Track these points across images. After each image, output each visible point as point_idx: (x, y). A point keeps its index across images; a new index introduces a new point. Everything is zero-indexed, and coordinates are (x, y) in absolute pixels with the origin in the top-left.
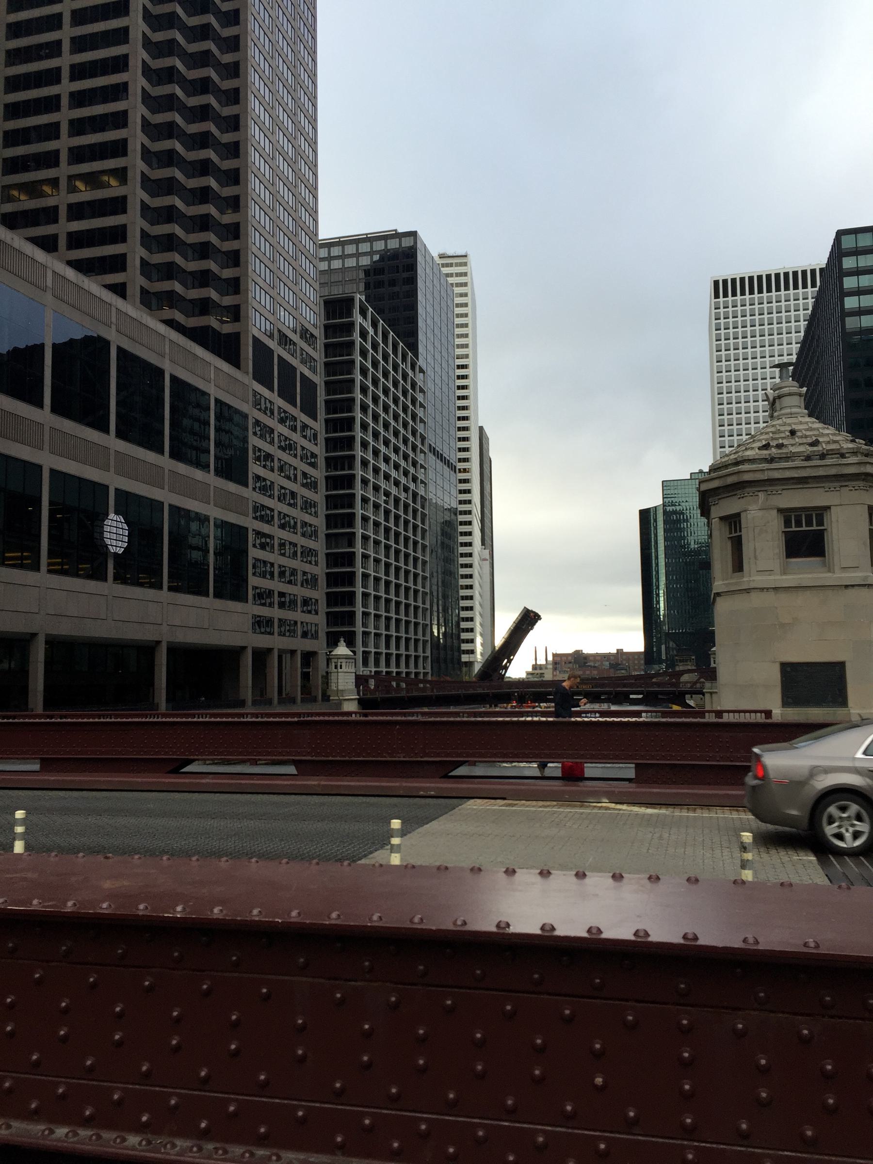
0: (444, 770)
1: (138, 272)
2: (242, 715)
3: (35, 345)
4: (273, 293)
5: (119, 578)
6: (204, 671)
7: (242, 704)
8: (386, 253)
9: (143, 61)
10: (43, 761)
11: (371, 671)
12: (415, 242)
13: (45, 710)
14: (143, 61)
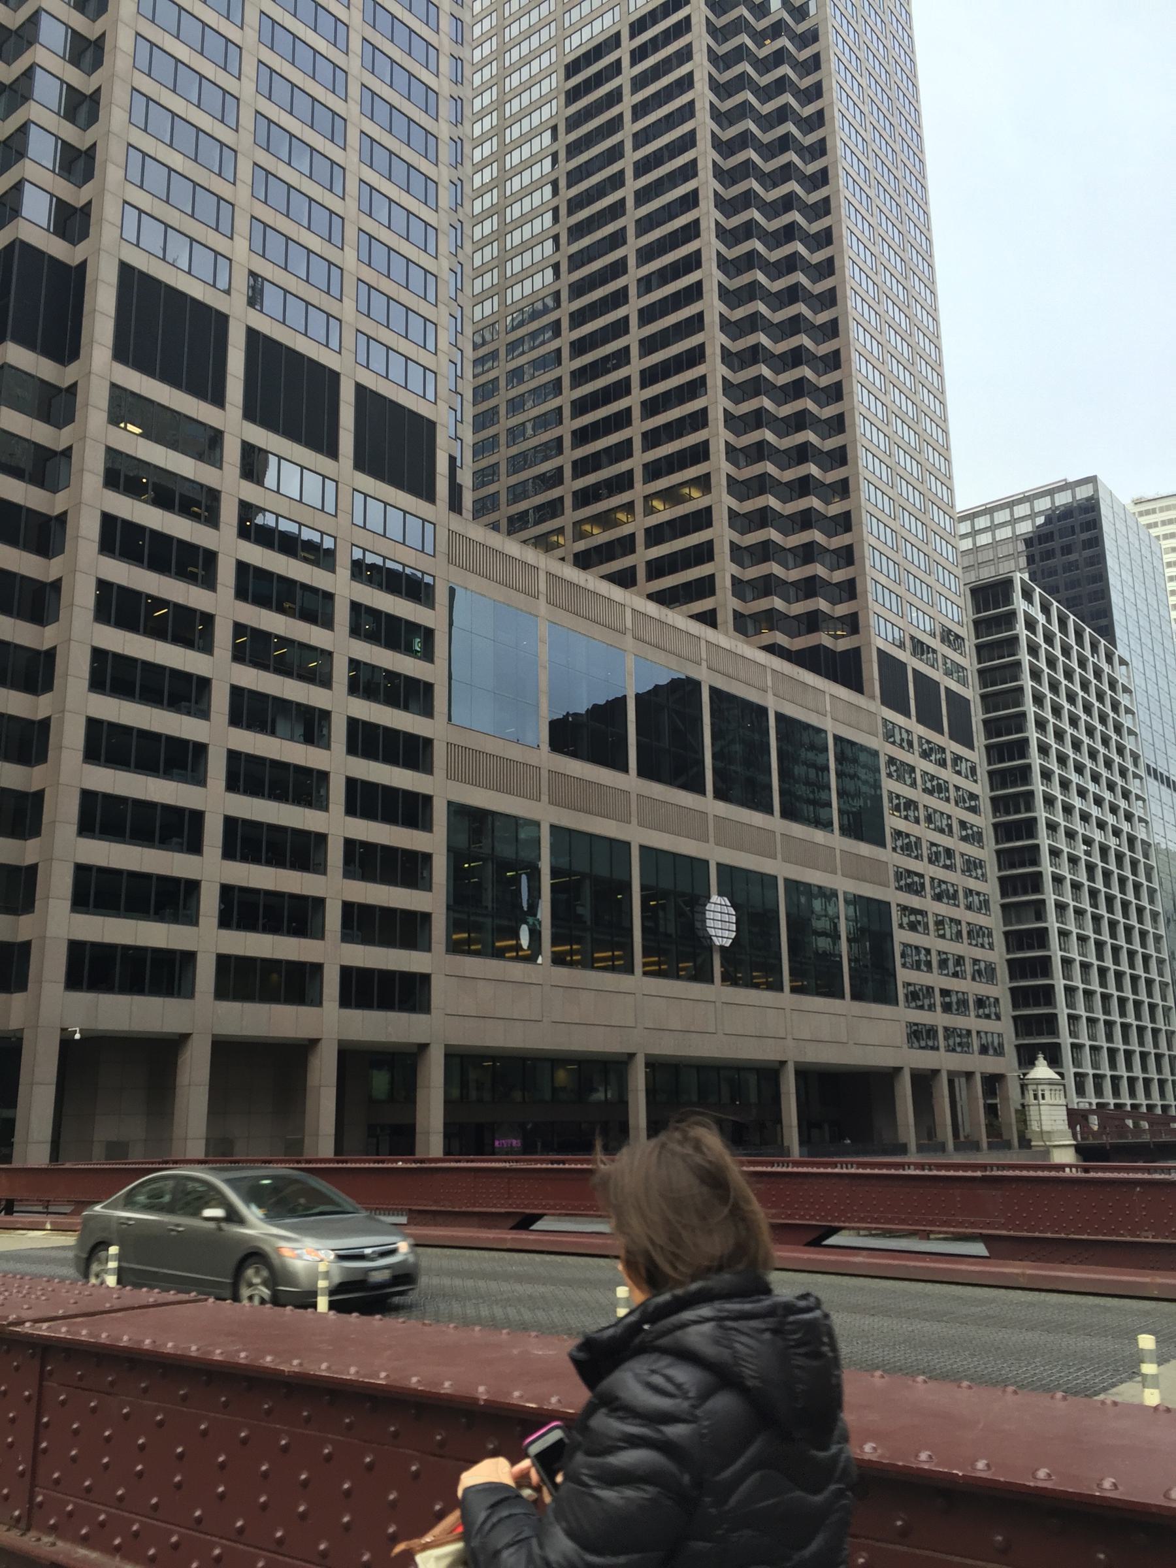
2: (902, 1166)
3: (617, 699)
4: (930, 580)
5: (730, 979)
8: (1054, 511)
11: (1090, 1104)
12: (1096, 490)
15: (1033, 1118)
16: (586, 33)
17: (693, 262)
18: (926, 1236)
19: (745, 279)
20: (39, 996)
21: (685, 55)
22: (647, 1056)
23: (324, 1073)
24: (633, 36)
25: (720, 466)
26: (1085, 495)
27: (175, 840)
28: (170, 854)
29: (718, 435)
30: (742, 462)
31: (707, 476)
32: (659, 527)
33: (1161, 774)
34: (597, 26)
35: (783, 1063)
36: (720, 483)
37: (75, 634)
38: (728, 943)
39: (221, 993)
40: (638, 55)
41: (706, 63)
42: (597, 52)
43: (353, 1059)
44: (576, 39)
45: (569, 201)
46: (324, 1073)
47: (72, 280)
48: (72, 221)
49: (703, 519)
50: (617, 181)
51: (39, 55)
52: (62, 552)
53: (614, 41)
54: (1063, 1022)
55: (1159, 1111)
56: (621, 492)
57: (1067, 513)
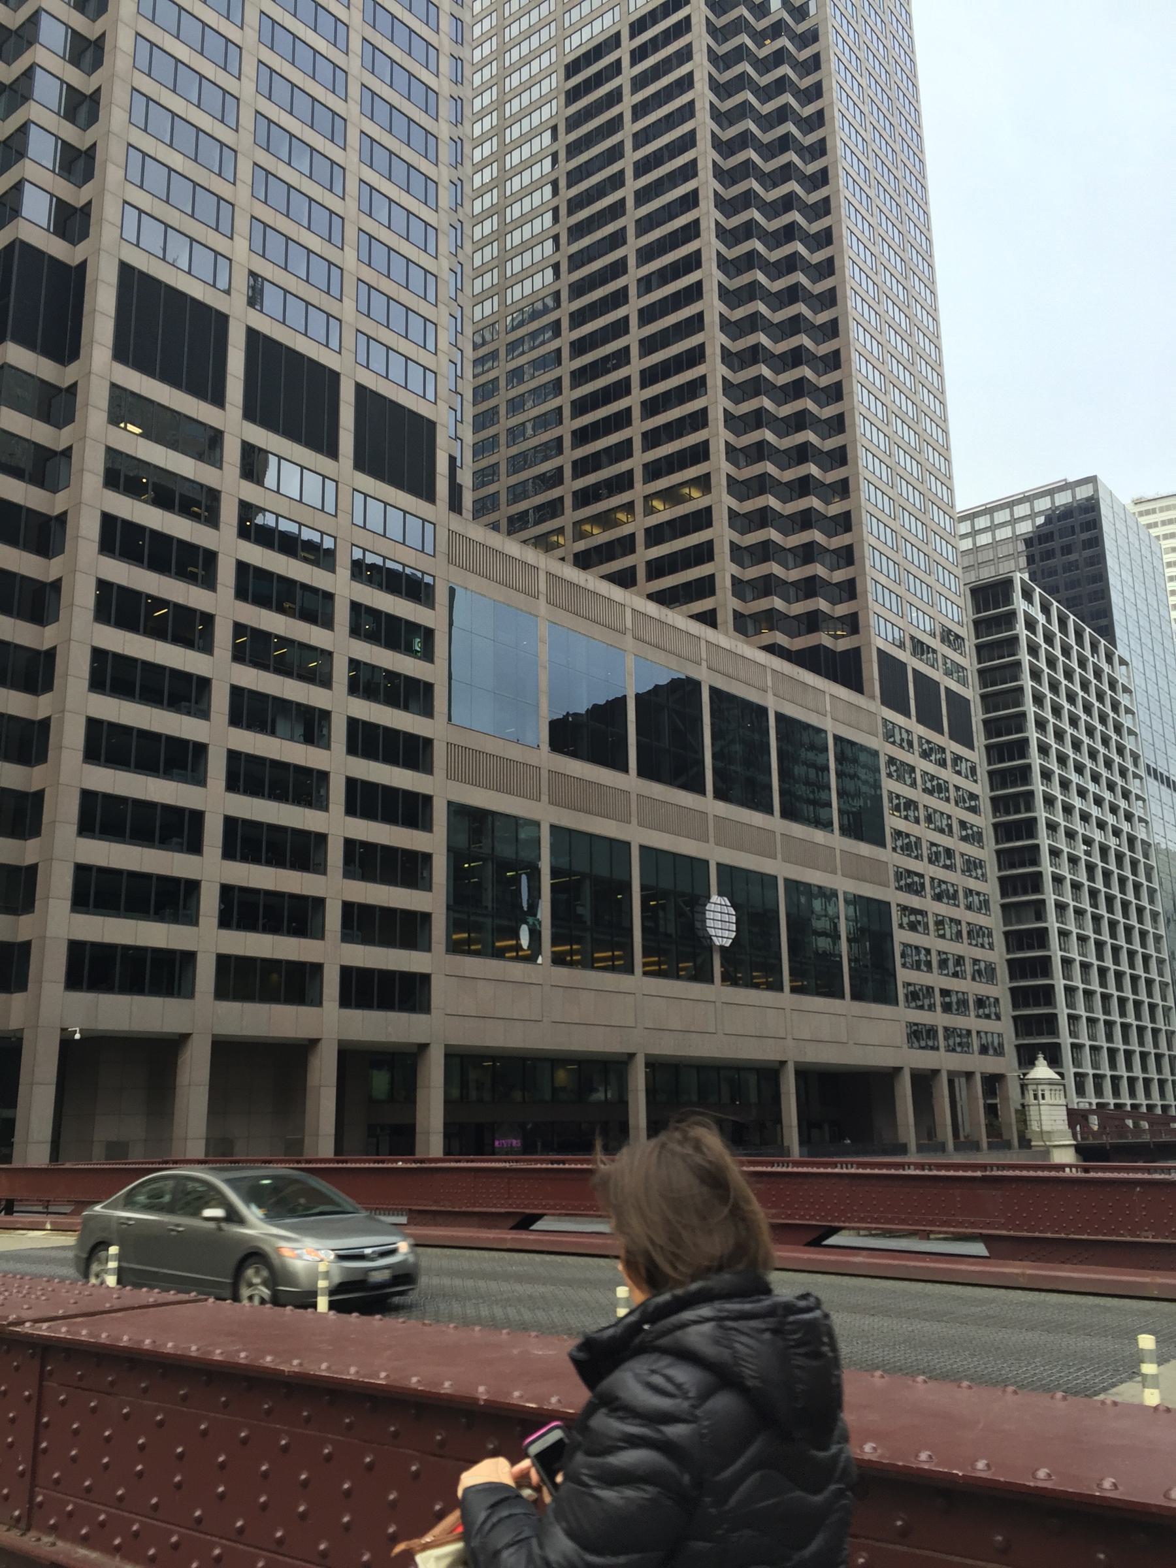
2: (902, 1166)
3: (617, 699)
4: (930, 580)
5: (730, 979)
8: (1054, 511)
11: (1090, 1104)
12: (1096, 490)
15: (1033, 1118)
16: (586, 33)
17: (693, 262)
18: (926, 1236)
19: (745, 279)
20: (39, 996)
21: (685, 55)
24: (633, 36)
25: (720, 466)
26: (1085, 495)
27: (175, 840)
28: (170, 854)
29: (718, 435)
30: (742, 462)
31: (707, 476)
32: (659, 527)
33: (1161, 774)
34: (597, 26)
35: (783, 1063)
36: (720, 483)
37: (75, 634)
38: (728, 943)
39: (221, 993)
40: (638, 55)
41: (706, 63)
42: (597, 52)
44: (576, 39)
45: (569, 201)
47: (72, 280)
48: (72, 221)
49: (703, 519)
50: (617, 181)
51: (39, 55)
52: (62, 552)
53: (614, 41)
54: (1063, 1022)
55: (1159, 1111)
56: (621, 492)
57: (1067, 513)
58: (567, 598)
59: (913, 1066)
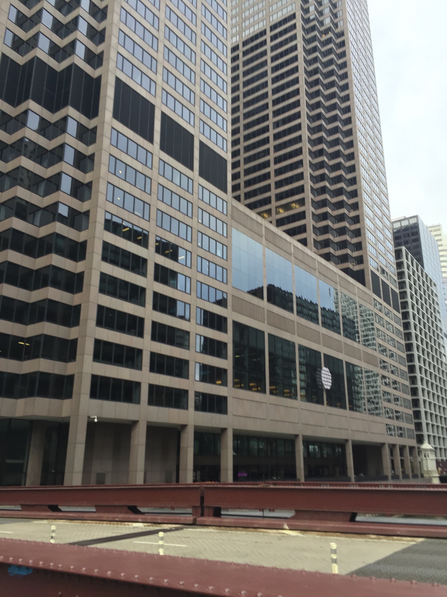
0: (55, 509)
1: (313, 245)
2: (386, 486)
5: (330, 404)
6: (327, 458)
7: (386, 478)
9: (309, 149)
10: (297, 511)
12: (417, 220)
13: (305, 480)
14: (309, 149)
16: (252, 30)
17: (298, 116)
18: (390, 515)
19: (317, 123)
20: (79, 401)
21: (294, 37)
22: (234, 430)
23: (139, 438)
25: (308, 195)
27: (133, 330)
28: (131, 336)
29: (308, 183)
35: (297, 436)
36: (308, 202)
38: (329, 388)
42: (256, 37)
43: (154, 430)
44: (247, 32)
46: (139, 438)
47: (95, 85)
48: (94, 59)
49: (302, 216)
53: (263, 33)
57: (407, 229)
58: (272, 240)
59: (236, 427)
